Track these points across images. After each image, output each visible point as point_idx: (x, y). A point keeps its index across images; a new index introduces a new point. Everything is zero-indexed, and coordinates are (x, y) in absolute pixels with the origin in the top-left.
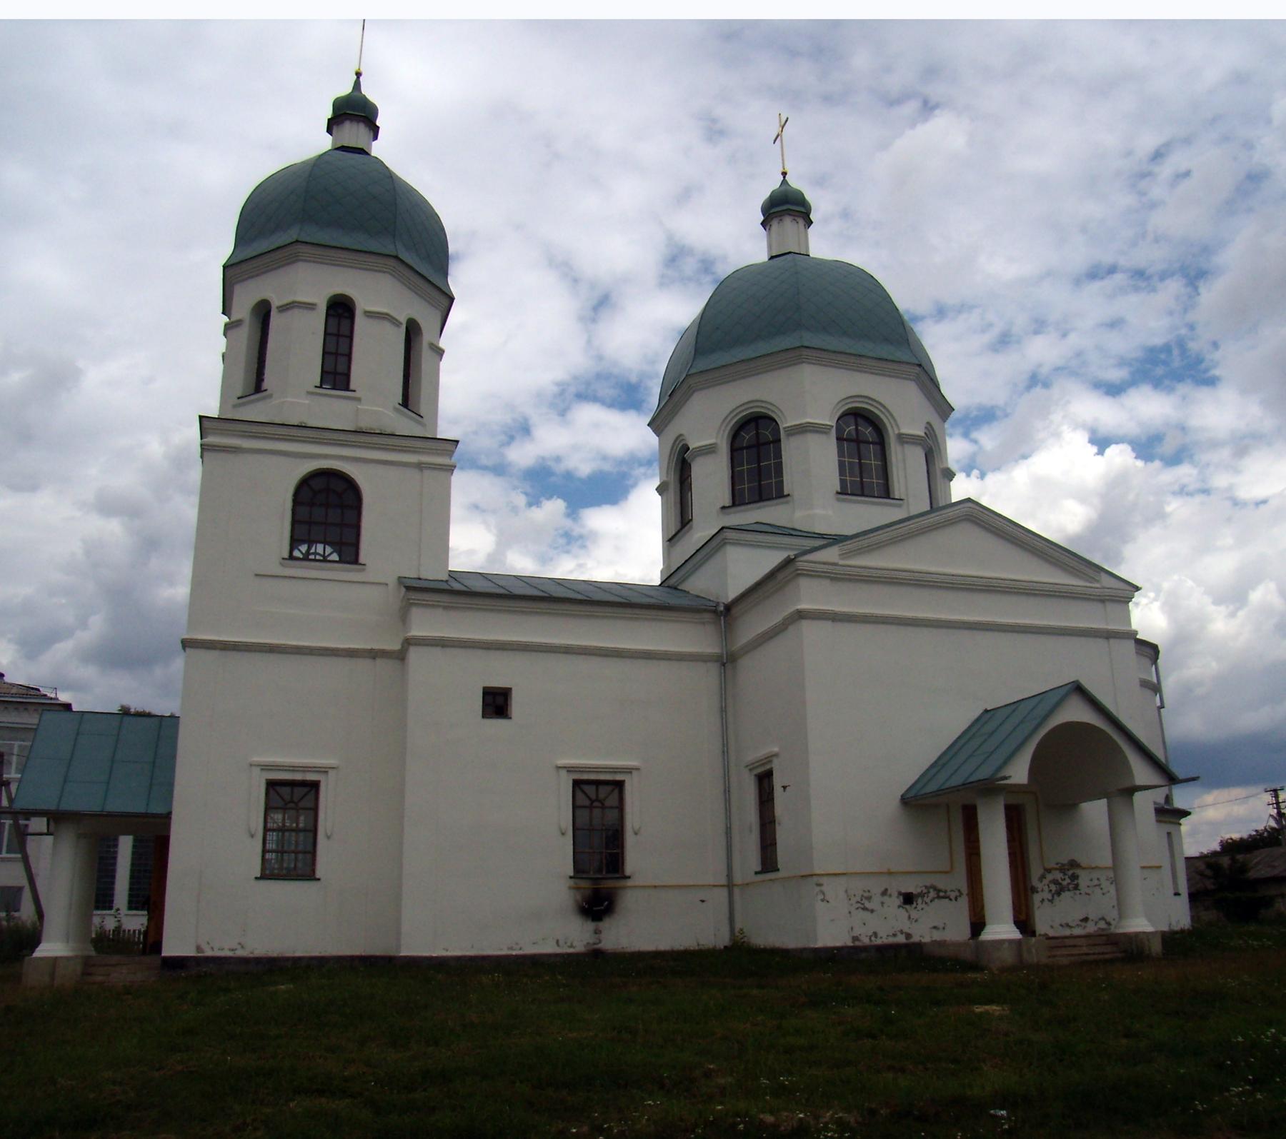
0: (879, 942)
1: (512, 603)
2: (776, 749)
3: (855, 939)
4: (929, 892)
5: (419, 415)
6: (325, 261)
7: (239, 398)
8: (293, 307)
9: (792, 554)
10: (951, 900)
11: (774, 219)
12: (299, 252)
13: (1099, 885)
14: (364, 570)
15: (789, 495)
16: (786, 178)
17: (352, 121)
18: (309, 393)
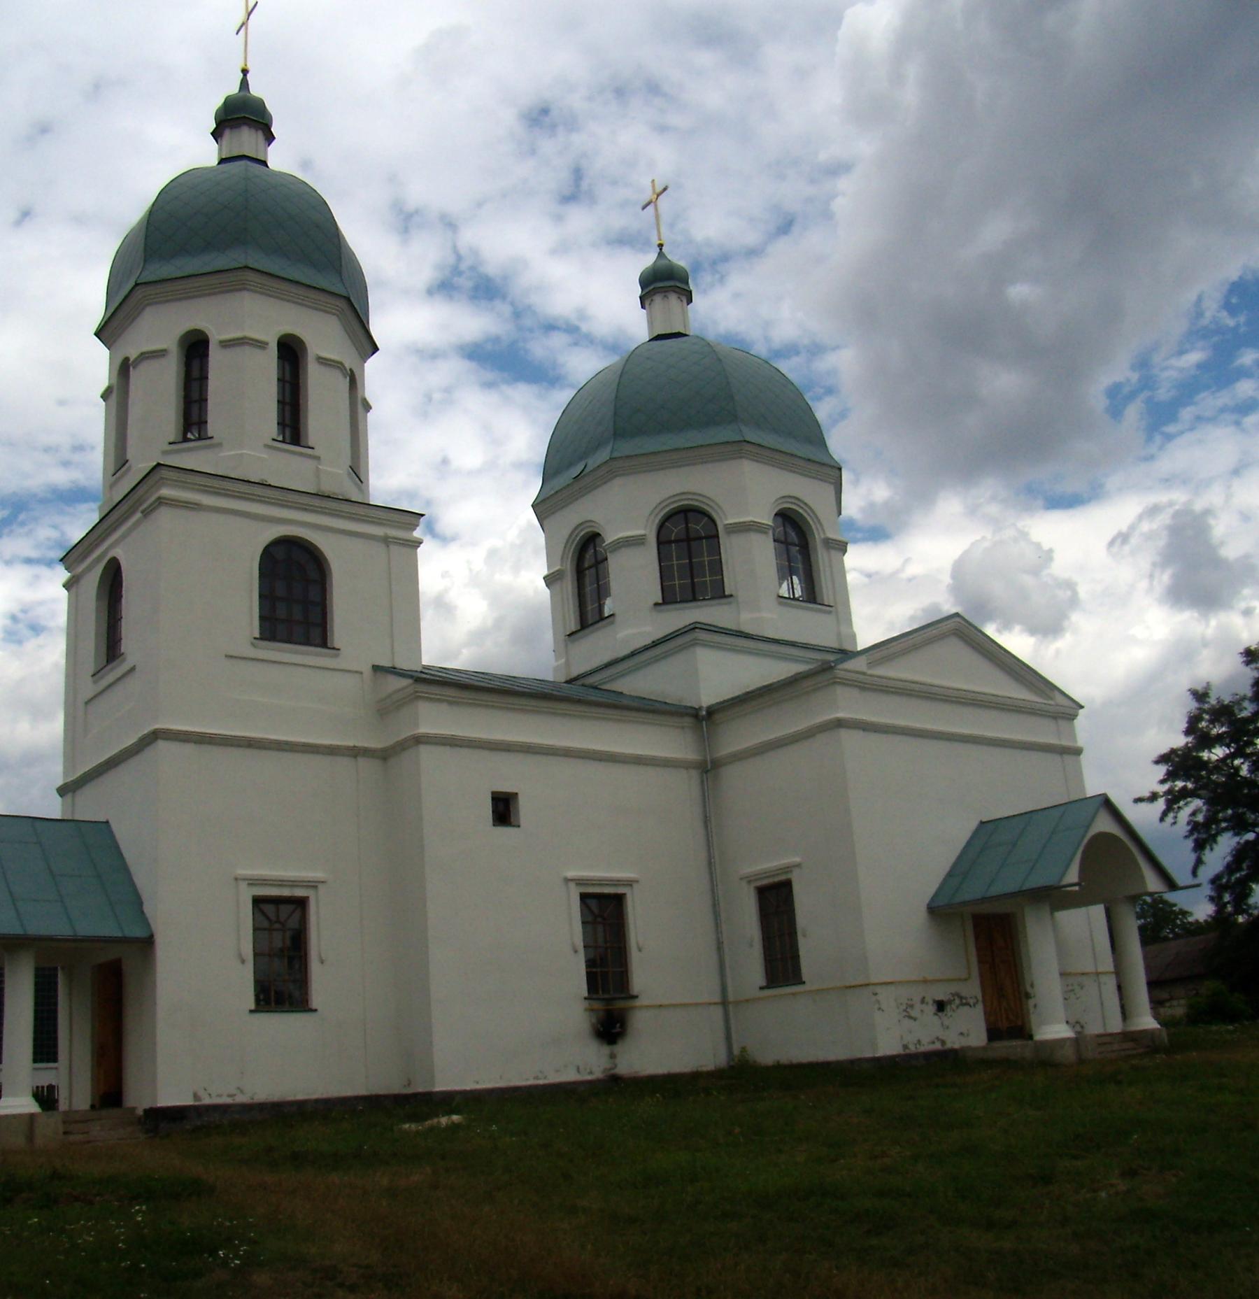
0: (922, 1049)
1: (511, 700)
2: (797, 859)
3: (905, 1047)
4: (954, 1000)
5: (360, 479)
6: (282, 296)
7: (170, 443)
8: (243, 344)
10: (971, 1006)
11: (658, 295)
12: (247, 280)
13: (1073, 990)
14: (337, 656)
15: (731, 596)
16: (663, 250)
17: (250, 126)
18: (267, 446)
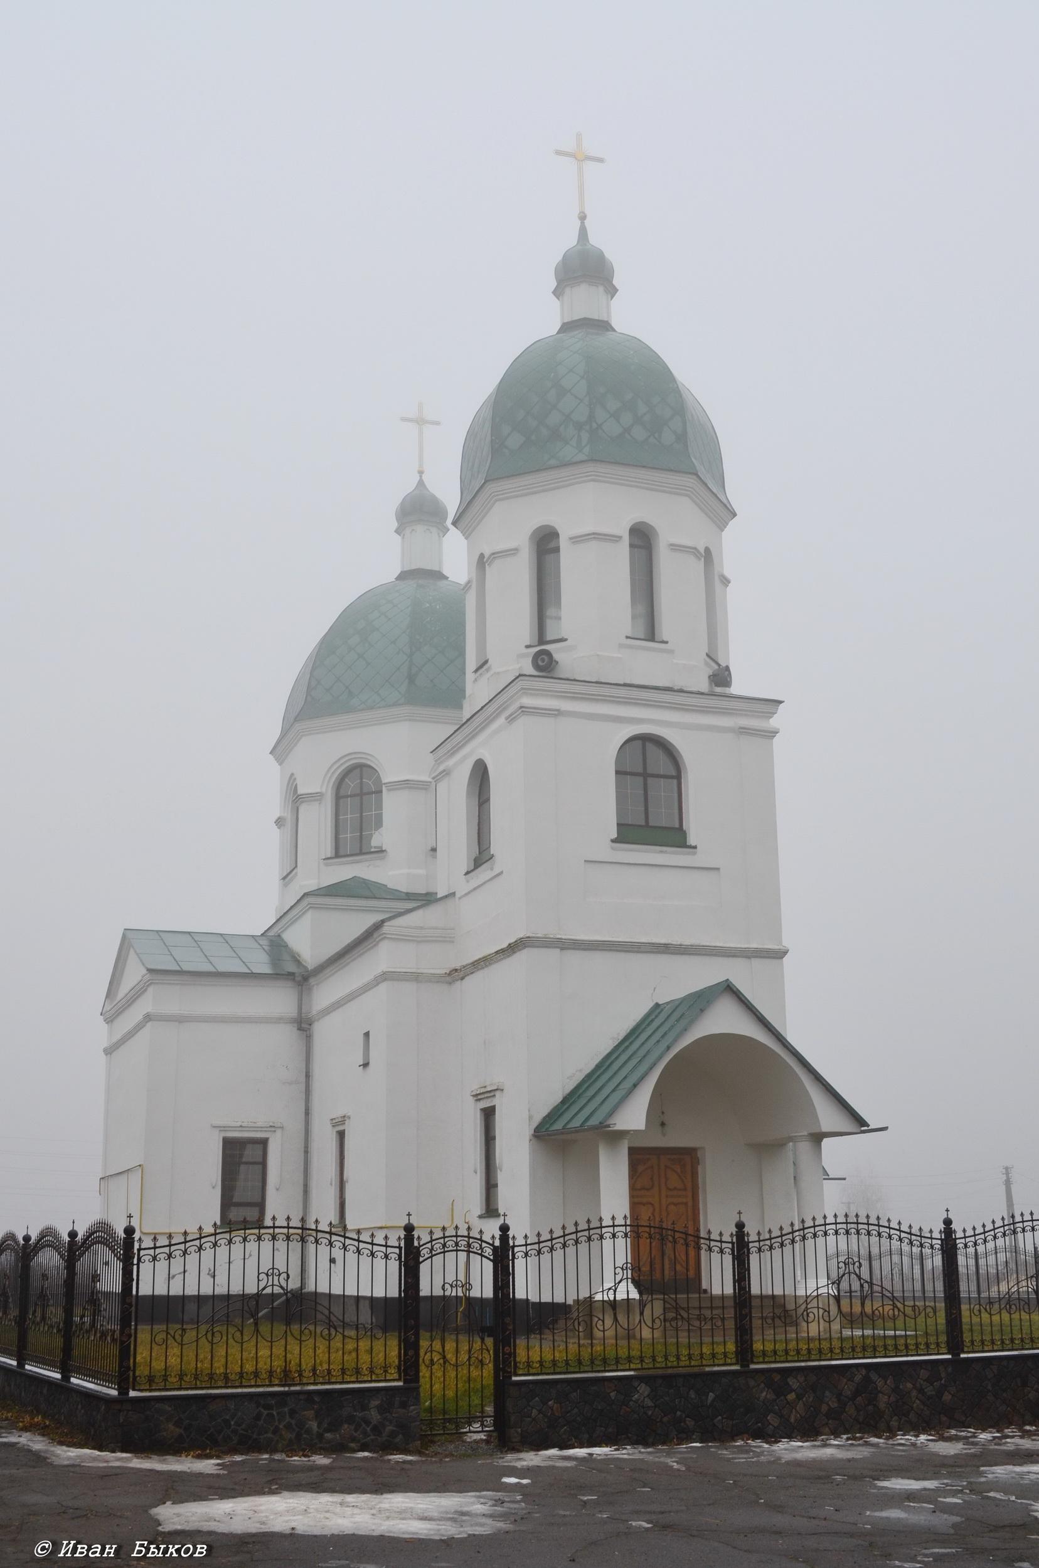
9: (381, 917)
